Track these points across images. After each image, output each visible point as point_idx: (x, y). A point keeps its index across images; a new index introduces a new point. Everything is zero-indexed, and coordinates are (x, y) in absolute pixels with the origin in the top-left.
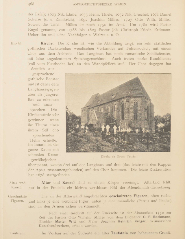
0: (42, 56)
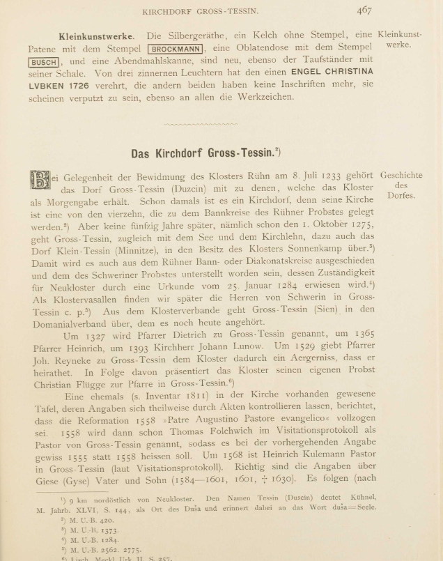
0: (118, 343)
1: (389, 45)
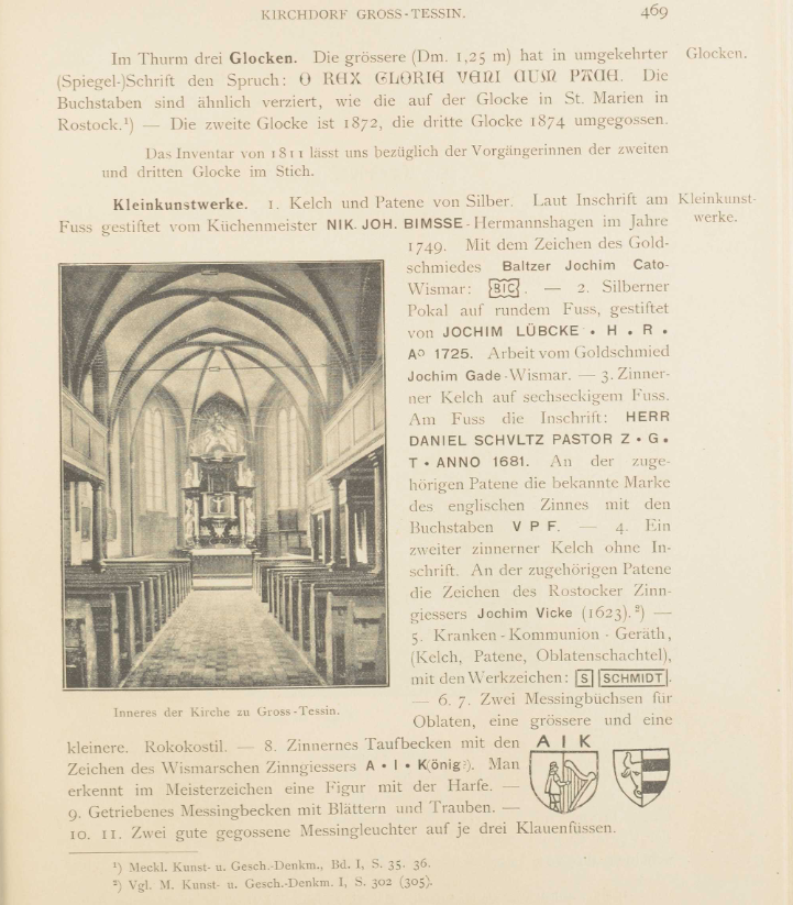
1: (698, 218)
